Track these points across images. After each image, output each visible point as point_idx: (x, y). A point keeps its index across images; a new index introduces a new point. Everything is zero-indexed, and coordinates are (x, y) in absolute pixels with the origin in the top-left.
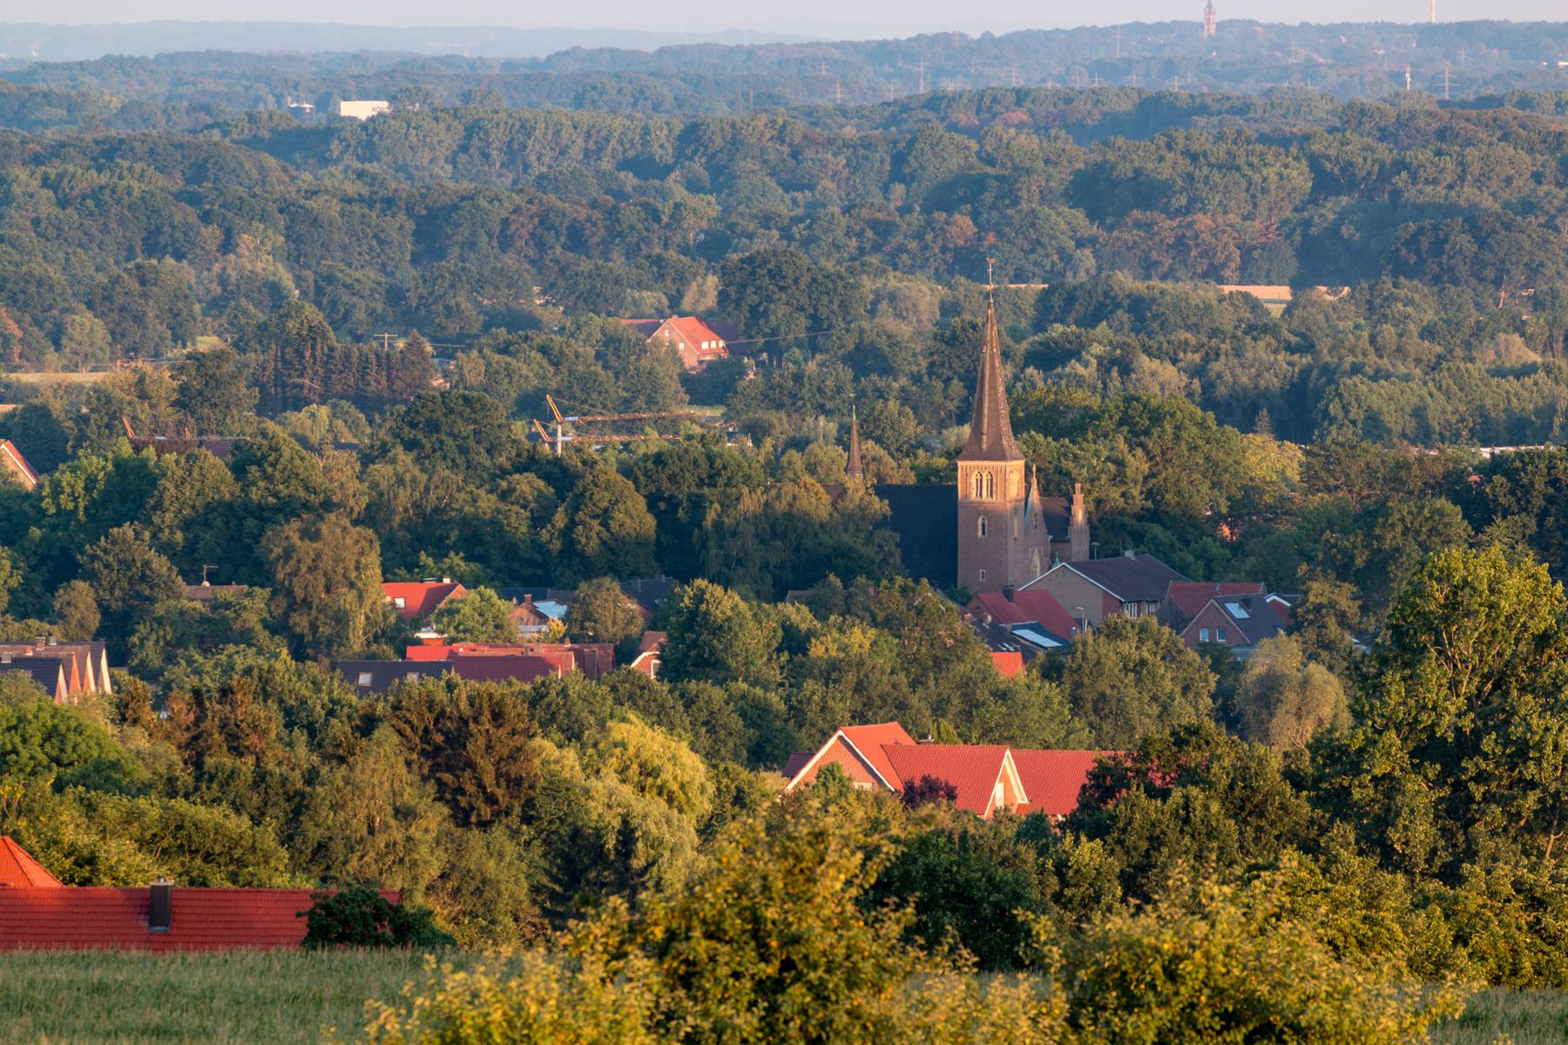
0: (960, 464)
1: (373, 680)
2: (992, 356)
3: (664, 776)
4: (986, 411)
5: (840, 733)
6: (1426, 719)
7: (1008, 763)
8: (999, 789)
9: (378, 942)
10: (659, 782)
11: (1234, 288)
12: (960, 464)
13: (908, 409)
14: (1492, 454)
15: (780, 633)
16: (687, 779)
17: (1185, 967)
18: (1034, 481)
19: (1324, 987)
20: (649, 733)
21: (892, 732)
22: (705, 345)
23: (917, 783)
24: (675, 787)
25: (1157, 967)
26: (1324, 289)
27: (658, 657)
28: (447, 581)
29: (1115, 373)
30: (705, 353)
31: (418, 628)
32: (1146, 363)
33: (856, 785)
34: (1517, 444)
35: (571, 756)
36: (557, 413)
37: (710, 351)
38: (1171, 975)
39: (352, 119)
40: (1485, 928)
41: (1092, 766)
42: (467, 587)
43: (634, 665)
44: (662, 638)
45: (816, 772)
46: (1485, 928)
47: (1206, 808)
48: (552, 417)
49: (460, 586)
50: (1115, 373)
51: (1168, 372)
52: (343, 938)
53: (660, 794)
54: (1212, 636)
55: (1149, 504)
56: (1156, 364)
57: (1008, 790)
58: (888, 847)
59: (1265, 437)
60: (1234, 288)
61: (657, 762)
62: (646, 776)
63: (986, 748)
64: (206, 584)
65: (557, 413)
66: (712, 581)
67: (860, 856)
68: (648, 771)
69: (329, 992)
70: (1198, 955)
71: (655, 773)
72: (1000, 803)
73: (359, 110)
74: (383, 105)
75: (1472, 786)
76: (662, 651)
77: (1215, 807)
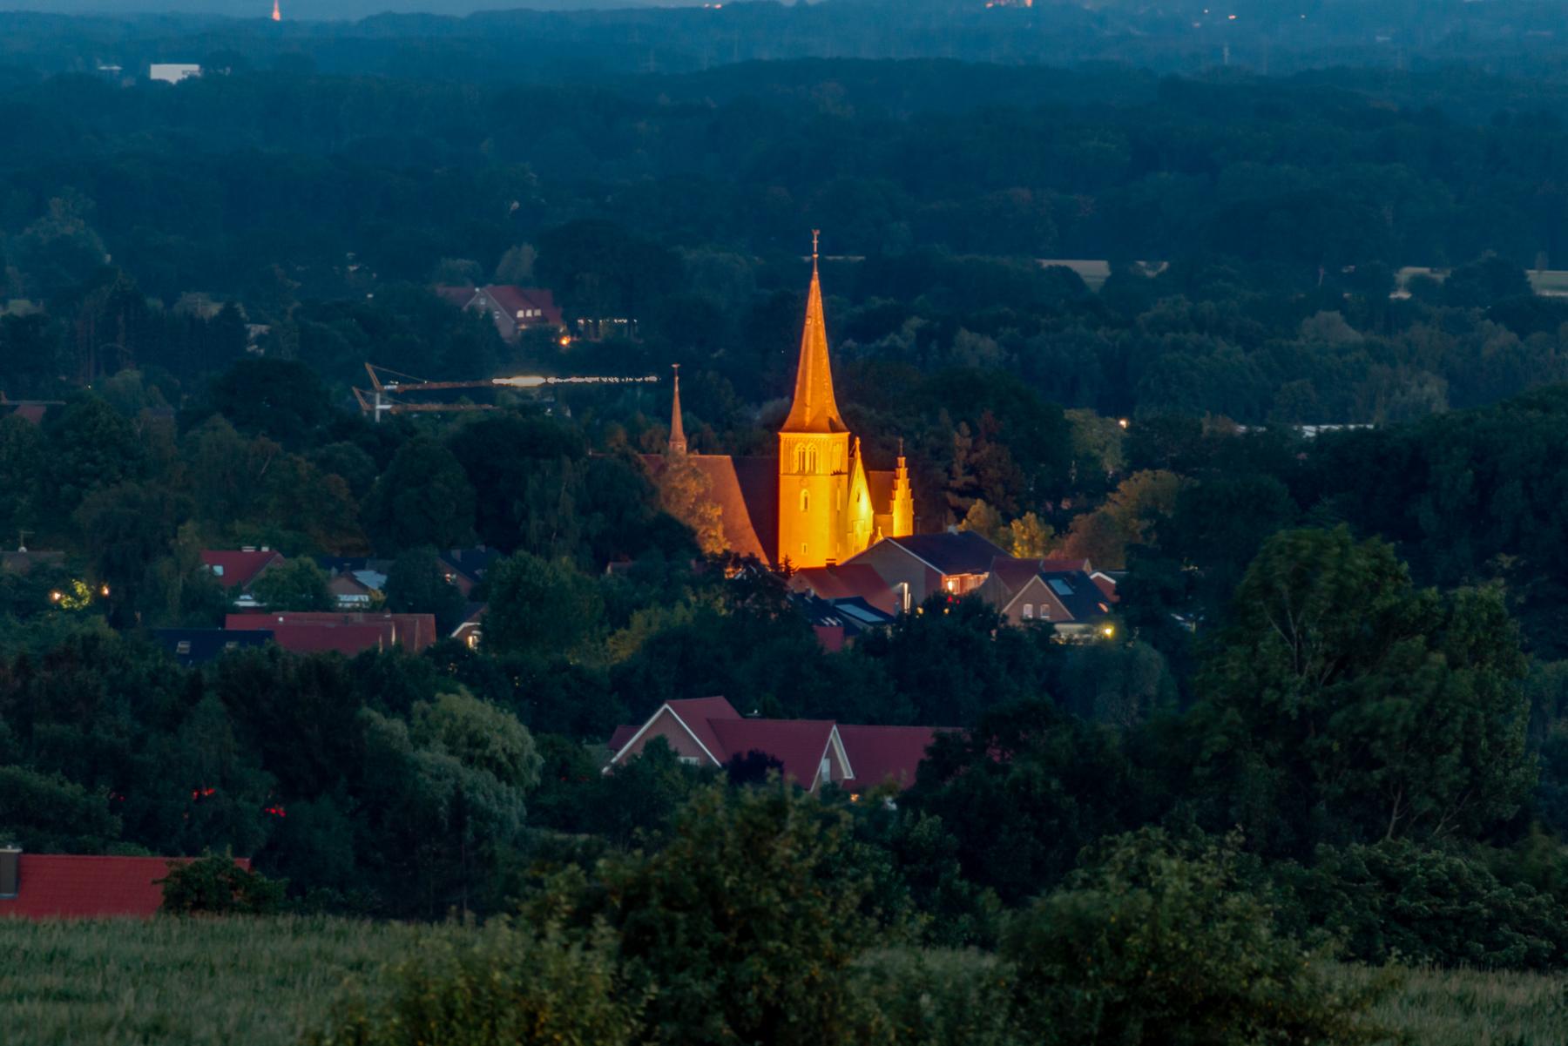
0: (783, 435)
1: (192, 649)
2: (816, 328)
3: (492, 747)
4: (809, 383)
5: (666, 706)
6: (1269, 694)
7: (835, 737)
8: (825, 766)
9: (234, 909)
10: (487, 753)
11: (1053, 262)
12: (783, 435)
13: (727, 381)
14: (1318, 432)
15: (602, 605)
16: (516, 751)
17: (1133, 941)
18: (858, 454)
19: (1271, 962)
20: (478, 703)
21: (719, 706)
22: (520, 314)
23: (745, 757)
24: (504, 759)
25: (1103, 939)
26: (1142, 263)
27: (480, 628)
28: (265, 549)
29: (934, 346)
30: (519, 322)
31: (237, 597)
32: (965, 336)
33: (682, 759)
34: (1343, 420)
35: (398, 726)
36: (376, 383)
37: (525, 320)
38: (1118, 948)
39: (163, 83)
40: (1340, 907)
41: (931, 742)
42: (286, 556)
43: (454, 634)
44: (484, 609)
45: (642, 746)
46: (1340, 907)
47: (1047, 784)
48: (371, 385)
49: (279, 555)
50: (934, 346)
51: (988, 345)
52: (199, 906)
53: (489, 766)
54: (1036, 610)
55: (972, 479)
56: (975, 337)
57: (835, 765)
58: (847, 816)
59: (1087, 412)
60: (1053, 262)
61: (486, 734)
62: (473, 748)
63: (815, 725)
64: (23, 549)
65: (376, 383)
66: (534, 553)
67: (817, 824)
68: (476, 742)
69: (217, 961)
70: (1145, 928)
71: (484, 743)
72: (827, 779)
73: (169, 73)
74: (194, 68)
75: (1315, 764)
76: (483, 622)
77: (1055, 784)
